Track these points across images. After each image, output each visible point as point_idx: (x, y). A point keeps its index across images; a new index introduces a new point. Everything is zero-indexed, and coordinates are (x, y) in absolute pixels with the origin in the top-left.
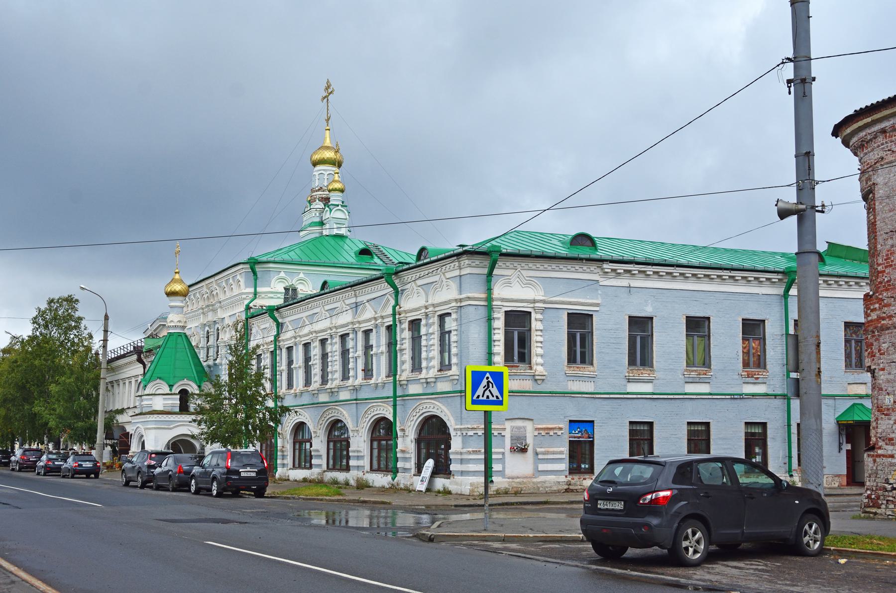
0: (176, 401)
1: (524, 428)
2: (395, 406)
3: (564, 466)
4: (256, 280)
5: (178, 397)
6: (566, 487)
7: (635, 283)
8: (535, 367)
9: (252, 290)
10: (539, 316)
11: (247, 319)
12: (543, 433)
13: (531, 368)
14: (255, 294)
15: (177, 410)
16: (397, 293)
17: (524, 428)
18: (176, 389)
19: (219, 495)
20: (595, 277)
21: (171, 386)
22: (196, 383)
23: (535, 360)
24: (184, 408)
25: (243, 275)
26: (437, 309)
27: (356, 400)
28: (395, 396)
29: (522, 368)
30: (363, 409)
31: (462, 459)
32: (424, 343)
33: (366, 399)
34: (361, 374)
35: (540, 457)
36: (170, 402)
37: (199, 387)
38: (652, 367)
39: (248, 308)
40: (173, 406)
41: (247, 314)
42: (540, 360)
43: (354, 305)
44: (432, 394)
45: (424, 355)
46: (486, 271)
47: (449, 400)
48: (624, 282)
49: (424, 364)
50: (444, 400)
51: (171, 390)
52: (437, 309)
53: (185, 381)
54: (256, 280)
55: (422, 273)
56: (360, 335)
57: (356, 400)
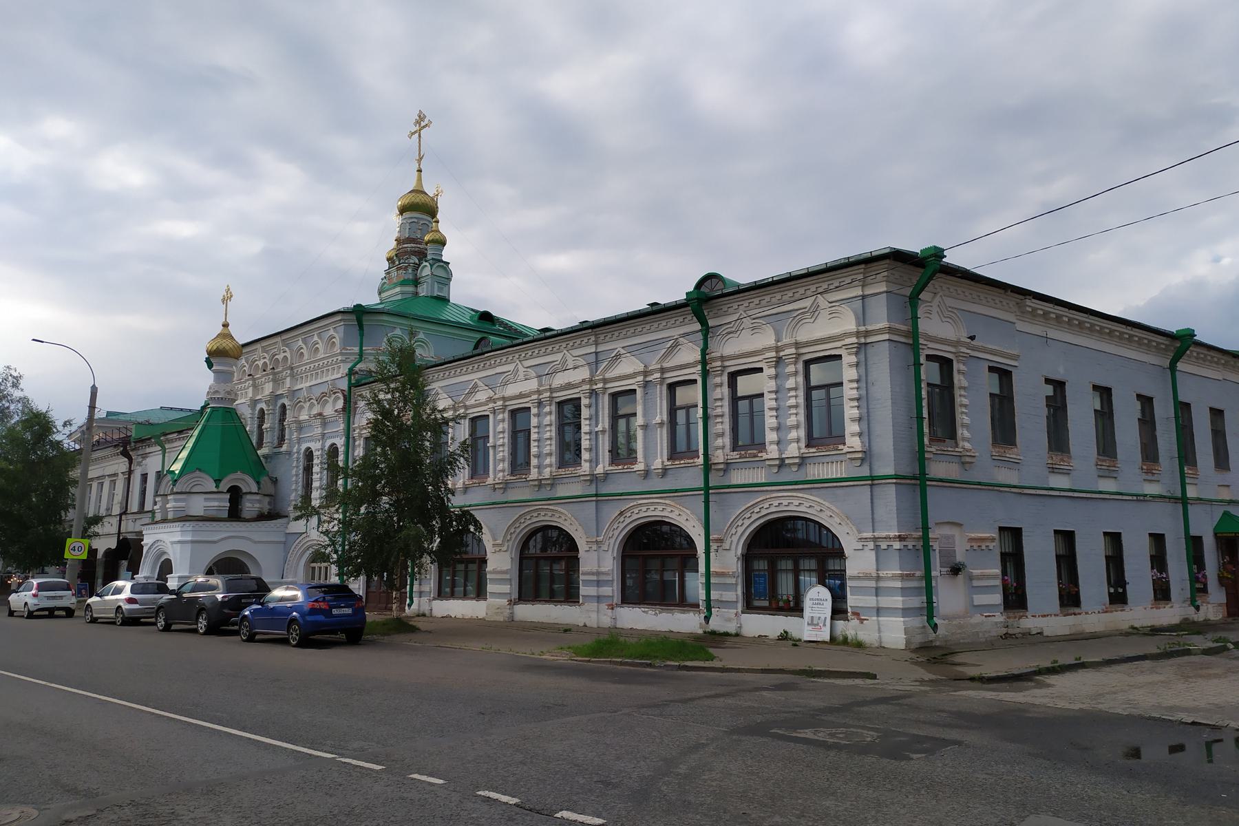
0: (223, 503)
1: (953, 536)
2: (707, 502)
3: (997, 598)
4: (362, 335)
5: (228, 496)
6: (1004, 631)
7: (1053, 334)
8: (961, 444)
9: (356, 350)
10: (962, 367)
11: (350, 388)
12: (975, 545)
13: (957, 446)
14: (361, 354)
15: (226, 515)
16: (706, 331)
17: (953, 536)
18: (224, 486)
19: (205, 634)
20: (1012, 318)
21: (218, 482)
22: (254, 479)
23: (962, 432)
24: (235, 514)
25: (341, 329)
26: (727, 363)
27: (596, 495)
28: (707, 488)
29: (948, 446)
30: (611, 511)
31: (598, 581)
32: (534, 436)
33: (621, 494)
34: (605, 456)
35: (975, 583)
36: (216, 504)
37: (258, 483)
38: (1069, 452)
39: (351, 372)
40: (219, 509)
41: (350, 380)
42: (966, 434)
43: (592, 358)
44: (796, 483)
45: (534, 450)
46: (908, 291)
47: (839, 491)
48: (1037, 329)
49: (534, 461)
50: (823, 491)
51: (217, 487)
52: (727, 363)
53: (239, 475)
54: (362, 335)
55: (825, 286)
56: (605, 401)
57: (596, 495)
